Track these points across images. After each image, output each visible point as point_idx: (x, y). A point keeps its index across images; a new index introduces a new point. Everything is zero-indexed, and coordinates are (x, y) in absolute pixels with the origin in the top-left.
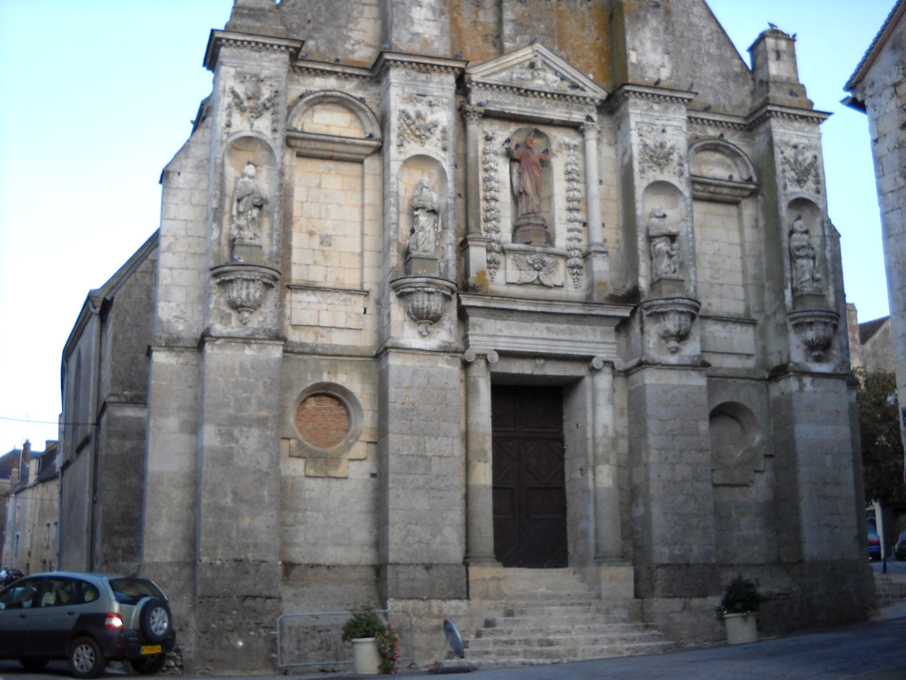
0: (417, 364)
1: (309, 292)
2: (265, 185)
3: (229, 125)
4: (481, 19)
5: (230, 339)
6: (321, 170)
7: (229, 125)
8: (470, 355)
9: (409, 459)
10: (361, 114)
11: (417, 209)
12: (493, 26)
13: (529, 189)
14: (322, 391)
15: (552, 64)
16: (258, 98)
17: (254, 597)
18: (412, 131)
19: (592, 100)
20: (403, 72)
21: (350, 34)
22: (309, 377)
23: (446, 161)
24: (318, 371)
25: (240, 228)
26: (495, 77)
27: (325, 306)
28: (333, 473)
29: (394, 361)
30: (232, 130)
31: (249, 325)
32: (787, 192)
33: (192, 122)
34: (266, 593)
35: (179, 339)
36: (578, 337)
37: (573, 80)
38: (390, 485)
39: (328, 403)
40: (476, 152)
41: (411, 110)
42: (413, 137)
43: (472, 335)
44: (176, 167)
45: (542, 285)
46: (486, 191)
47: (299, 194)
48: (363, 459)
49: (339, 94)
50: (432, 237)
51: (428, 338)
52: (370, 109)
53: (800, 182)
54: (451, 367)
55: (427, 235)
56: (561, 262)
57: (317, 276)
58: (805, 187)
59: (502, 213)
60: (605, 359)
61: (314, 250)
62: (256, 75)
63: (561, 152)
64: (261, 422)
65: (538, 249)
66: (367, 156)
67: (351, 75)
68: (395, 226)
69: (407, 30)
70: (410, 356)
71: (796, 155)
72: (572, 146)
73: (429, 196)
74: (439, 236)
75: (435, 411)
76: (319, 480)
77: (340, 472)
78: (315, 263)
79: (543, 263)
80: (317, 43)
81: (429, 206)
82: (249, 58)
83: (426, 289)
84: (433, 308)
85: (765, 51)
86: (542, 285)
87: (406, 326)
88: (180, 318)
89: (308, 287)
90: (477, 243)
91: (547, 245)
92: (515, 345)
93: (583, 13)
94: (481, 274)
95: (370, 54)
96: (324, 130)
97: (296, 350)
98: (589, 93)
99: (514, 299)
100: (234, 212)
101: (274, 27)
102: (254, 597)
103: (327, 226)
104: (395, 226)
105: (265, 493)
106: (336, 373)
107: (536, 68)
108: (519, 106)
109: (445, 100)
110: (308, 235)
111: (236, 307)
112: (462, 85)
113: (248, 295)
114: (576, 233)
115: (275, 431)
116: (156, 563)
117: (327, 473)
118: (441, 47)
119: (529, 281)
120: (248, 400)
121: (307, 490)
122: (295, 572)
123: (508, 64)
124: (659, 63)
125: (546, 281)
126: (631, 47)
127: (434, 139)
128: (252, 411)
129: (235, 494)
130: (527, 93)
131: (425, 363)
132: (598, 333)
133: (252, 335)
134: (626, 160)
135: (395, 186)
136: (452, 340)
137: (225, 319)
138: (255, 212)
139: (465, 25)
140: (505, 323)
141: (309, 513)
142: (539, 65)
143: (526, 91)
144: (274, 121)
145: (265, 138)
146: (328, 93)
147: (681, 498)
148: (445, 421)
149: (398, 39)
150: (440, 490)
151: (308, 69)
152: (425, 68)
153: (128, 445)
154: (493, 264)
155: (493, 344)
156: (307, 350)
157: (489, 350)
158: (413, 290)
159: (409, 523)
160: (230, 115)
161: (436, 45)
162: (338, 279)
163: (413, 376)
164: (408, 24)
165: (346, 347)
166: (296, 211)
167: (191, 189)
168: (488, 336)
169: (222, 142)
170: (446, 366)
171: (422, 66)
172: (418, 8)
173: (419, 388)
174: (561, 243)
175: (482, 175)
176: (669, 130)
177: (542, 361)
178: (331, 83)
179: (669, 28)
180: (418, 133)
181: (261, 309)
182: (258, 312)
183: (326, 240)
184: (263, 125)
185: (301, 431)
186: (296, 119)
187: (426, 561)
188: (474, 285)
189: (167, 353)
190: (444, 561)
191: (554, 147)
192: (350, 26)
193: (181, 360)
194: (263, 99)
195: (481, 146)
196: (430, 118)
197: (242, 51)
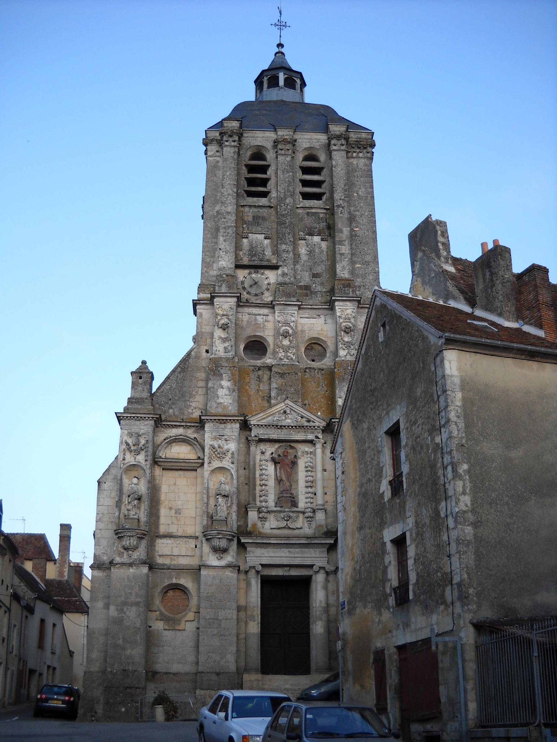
0: (215, 573)
1: (167, 538)
2: (143, 488)
3: (124, 459)
4: (261, 388)
5: (123, 564)
6: (176, 476)
7: (124, 459)
10: (194, 446)
11: (218, 495)
12: (267, 391)
13: (284, 478)
14: (174, 587)
15: (296, 410)
16: (139, 445)
17: (131, 688)
18: (216, 455)
19: (318, 427)
20: (212, 425)
21: (191, 404)
22: (166, 581)
24: (171, 578)
25: (128, 510)
26: (265, 421)
27: (175, 545)
28: (177, 628)
29: (203, 572)
30: (126, 462)
31: (132, 557)
34: (137, 686)
35: (103, 564)
36: (306, 555)
37: (308, 417)
39: (178, 593)
41: (216, 444)
44: (104, 480)
45: (289, 528)
46: (260, 481)
47: (164, 489)
48: (193, 621)
49: (183, 437)
50: (225, 508)
51: (221, 560)
54: (232, 574)
55: (222, 508)
56: (301, 515)
57: (173, 529)
59: (269, 492)
60: (320, 566)
62: (137, 433)
63: (303, 456)
64: (137, 604)
65: (286, 510)
66: (198, 467)
67: (190, 426)
69: (215, 402)
70: (212, 569)
72: (309, 452)
73: (224, 488)
74: (230, 507)
75: (224, 596)
76: (171, 631)
77: (181, 627)
78: (172, 523)
79: (290, 517)
81: (223, 493)
82: (134, 425)
83: (217, 536)
86: (289, 528)
87: (210, 555)
89: (169, 536)
90: (252, 509)
91: (292, 507)
93: (319, 378)
96: (176, 456)
97: (160, 567)
98: (317, 424)
101: (147, 407)
102: (131, 688)
103: (178, 504)
105: (138, 638)
106: (180, 578)
108: (277, 435)
111: (126, 549)
112: (245, 426)
113: (130, 543)
114: (309, 499)
115: (144, 608)
116: (91, 671)
117: (174, 628)
119: (283, 526)
120: (131, 593)
121: (165, 636)
122: (158, 676)
123: (271, 413)
126: (339, 396)
127: (227, 458)
128: (133, 599)
129: (124, 638)
131: (220, 573)
132: (318, 552)
133: (133, 562)
136: (234, 560)
137: (121, 554)
138: (136, 502)
140: (266, 550)
141: (165, 647)
142: (288, 412)
143: (281, 426)
144: (146, 456)
145: (141, 464)
146: (177, 437)
148: (229, 601)
149: (210, 407)
150: (225, 635)
151: (168, 425)
152: (224, 422)
154: (263, 519)
156: (166, 567)
157: (256, 564)
158: (211, 537)
159: (209, 652)
160: (124, 454)
162: (184, 531)
163: (213, 579)
164: (216, 398)
165: (186, 565)
166: (163, 497)
167: (111, 490)
168: (257, 557)
170: (230, 574)
171: (221, 421)
172: (222, 389)
173: (216, 585)
174: (302, 504)
175: (258, 473)
177: (288, 568)
178: (181, 431)
180: (218, 456)
181: (139, 550)
182: (137, 551)
183: (178, 512)
184: (141, 458)
186: (162, 452)
187: (218, 671)
188: (250, 531)
189: (98, 571)
190: (227, 671)
191: (299, 454)
192: (191, 400)
193: (105, 574)
194: (141, 445)
195: (258, 457)
196: (226, 447)
197: (130, 421)
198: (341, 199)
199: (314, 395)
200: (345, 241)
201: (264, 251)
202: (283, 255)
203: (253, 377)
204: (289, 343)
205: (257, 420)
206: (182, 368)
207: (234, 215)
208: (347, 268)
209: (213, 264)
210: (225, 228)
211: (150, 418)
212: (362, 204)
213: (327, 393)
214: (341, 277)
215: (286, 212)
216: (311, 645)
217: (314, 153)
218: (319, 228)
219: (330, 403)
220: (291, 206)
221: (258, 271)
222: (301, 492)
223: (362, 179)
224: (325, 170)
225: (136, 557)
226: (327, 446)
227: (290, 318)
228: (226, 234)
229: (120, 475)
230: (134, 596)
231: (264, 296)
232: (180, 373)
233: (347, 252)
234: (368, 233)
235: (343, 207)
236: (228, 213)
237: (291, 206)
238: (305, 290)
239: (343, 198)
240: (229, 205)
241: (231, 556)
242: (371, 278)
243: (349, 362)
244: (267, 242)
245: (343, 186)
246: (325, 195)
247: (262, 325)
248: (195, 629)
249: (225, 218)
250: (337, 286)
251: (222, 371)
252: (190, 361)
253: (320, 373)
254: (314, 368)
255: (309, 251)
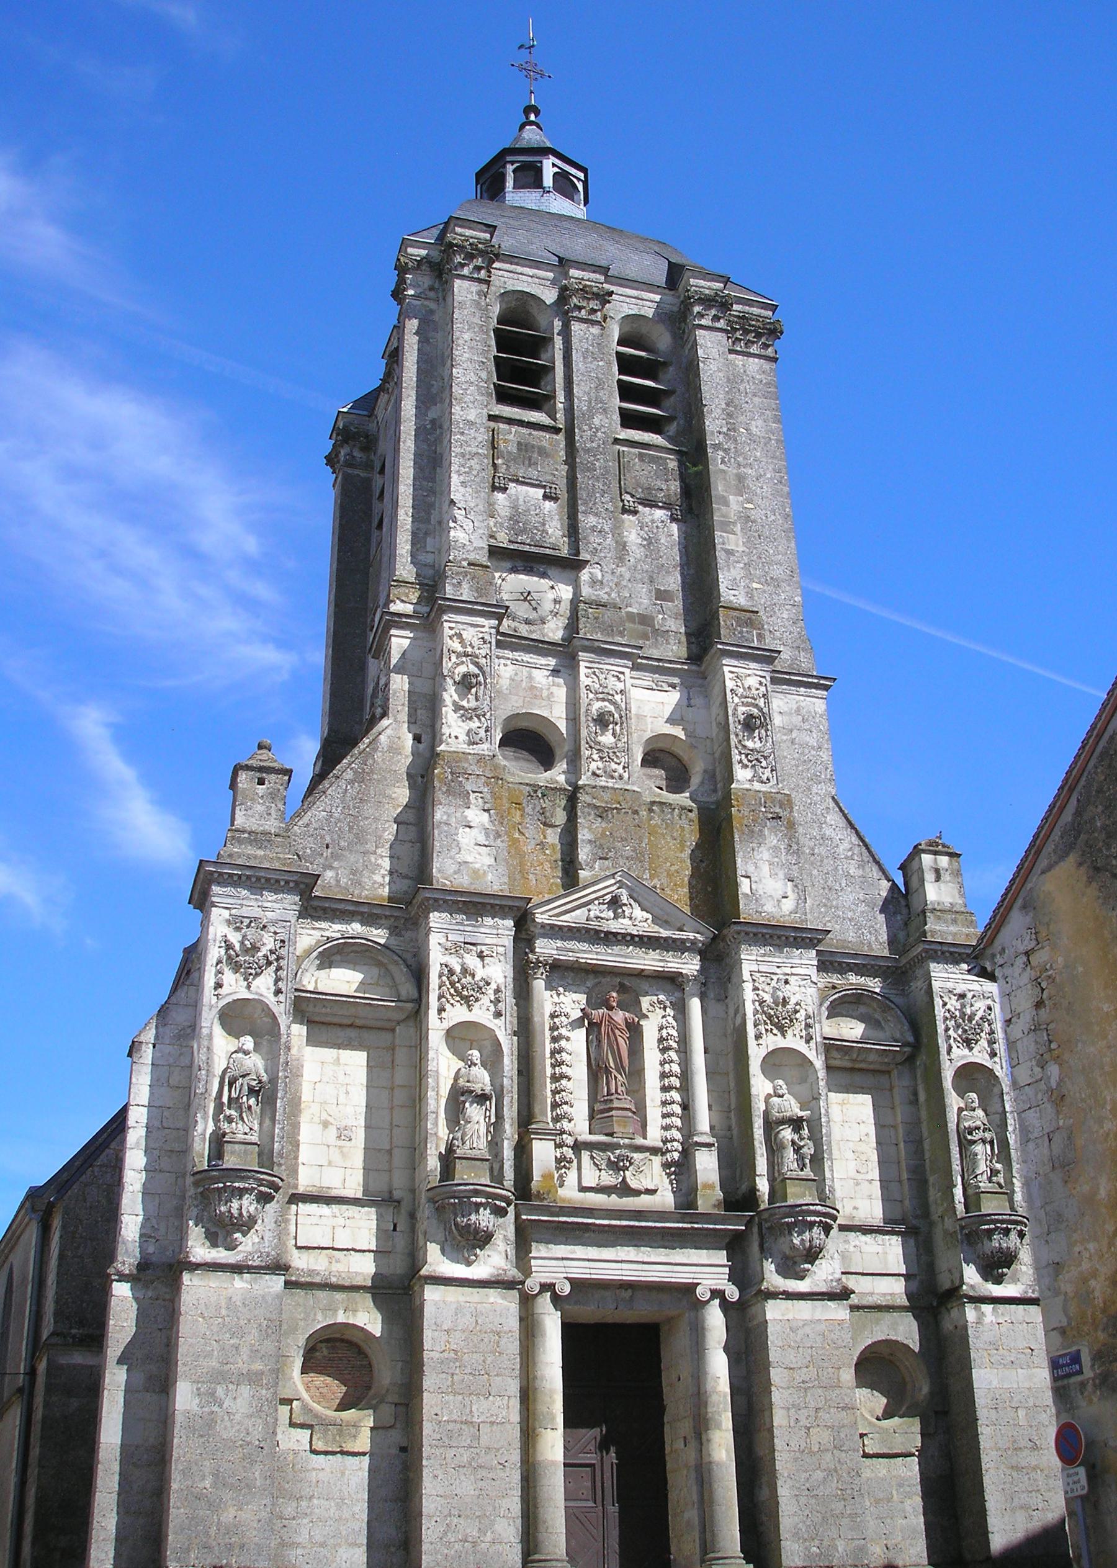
0: (462, 1299)
3: (218, 985)
8: (532, 1284)
9: (451, 1426)
21: (380, 861)
22: (319, 1317)
23: (503, 1032)
27: (341, 1221)
28: (348, 1447)
30: (222, 991)
32: (953, 1056)
33: (326, 464)
38: (424, 1463)
40: (543, 1014)
42: (458, 999)
43: (535, 1258)
48: (390, 1427)
52: (404, 961)
53: (968, 1043)
58: (976, 1049)
61: (328, 1146)
64: (253, 1379)
66: (398, 1023)
68: (434, 1115)
71: (963, 1006)
78: (330, 1164)
80: (337, 874)
84: (483, 1224)
85: (921, 870)
88: (150, 1237)
92: (592, 1271)
94: (548, 1177)
95: (405, 888)
99: (590, 1212)
100: (225, 1099)
101: (281, 856)
104: (434, 1115)
106: (355, 1311)
107: (620, 903)
109: (501, 950)
110: (321, 1126)
118: (495, 882)
124: (781, 893)
125: (633, 1184)
127: (485, 1000)
128: (242, 1363)
129: (216, 1475)
130: (610, 938)
134: (738, 1021)
135: (435, 1064)
139: (529, 847)
141: (315, 1501)
147: (819, 1475)
148: (497, 1375)
153: (75, 1403)
155: (563, 1270)
161: (490, 877)
164: (454, 851)
167: (169, 1065)
169: (211, 1007)
176: (792, 979)
179: (793, 846)
185: (308, 1389)
186: (308, 974)
198: (720, 433)
199: (673, 868)
200: (734, 523)
201: (544, 525)
202: (592, 539)
203: (529, 810)
204: (612, 740)
205: (550, 913)
206: (355, 772)
207: (482, 430)
208: (743, 584)
209: (425, 538)
210: (463, 455)
211: (292, 885)
212: (758, 454)
213: (704, 865)
214: (731, 602)
215: (594, 444)
216: (672, 1496)
217: (644, 330)
218: (668, 490)
219: (710, 889)
220: (604, 433)
221: (532, 568)
222: (652, 1100)
223: (756, 400)
224: (671, 369)
225: (249, 1248)
226: (708, 992)
227: (613, 684)
228: (467, 470)
229: (209, 1025)
230: (245, 1357)
231: (546, 626)
232: (351, 782)
233: (741, 549)
234: (773, 517)
235: (725, 450)
236: (471, 423)
237: (604, 433)
238: (640, 623)
239: (725, 430)
240: (471, 405)
241: (500, 1253)
242: (786, 616)
243: (761, 795)
244: (548, 505)
245: (724, 406)
246: (675, 424)
247: (545, 694)
248: (395, 1451)
249: (462, 433)
250: (724, 621)
251: (469, 786)
252: (378, 756)
253: (683, 817)
254: (670, 804)
255: (645, 539)
